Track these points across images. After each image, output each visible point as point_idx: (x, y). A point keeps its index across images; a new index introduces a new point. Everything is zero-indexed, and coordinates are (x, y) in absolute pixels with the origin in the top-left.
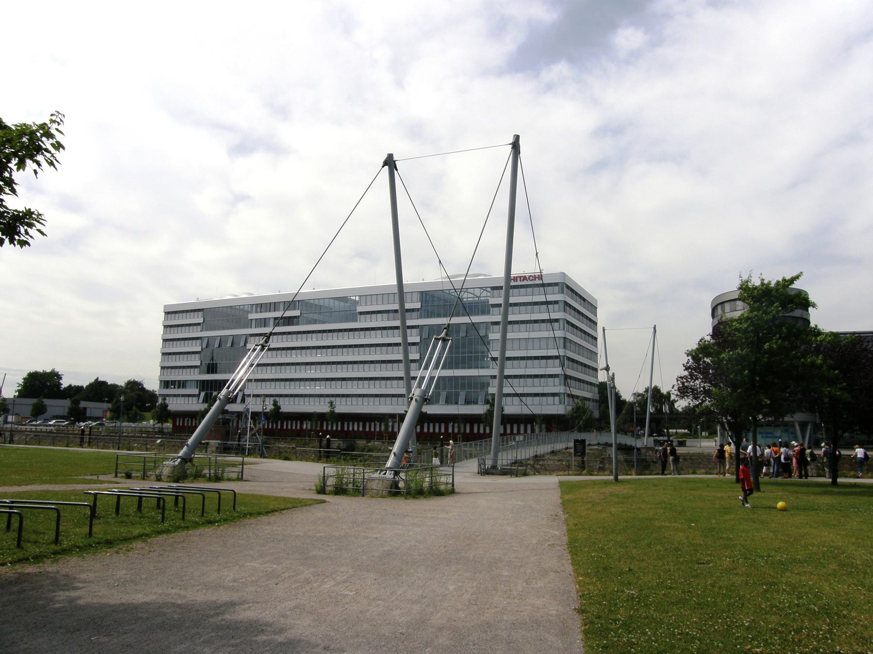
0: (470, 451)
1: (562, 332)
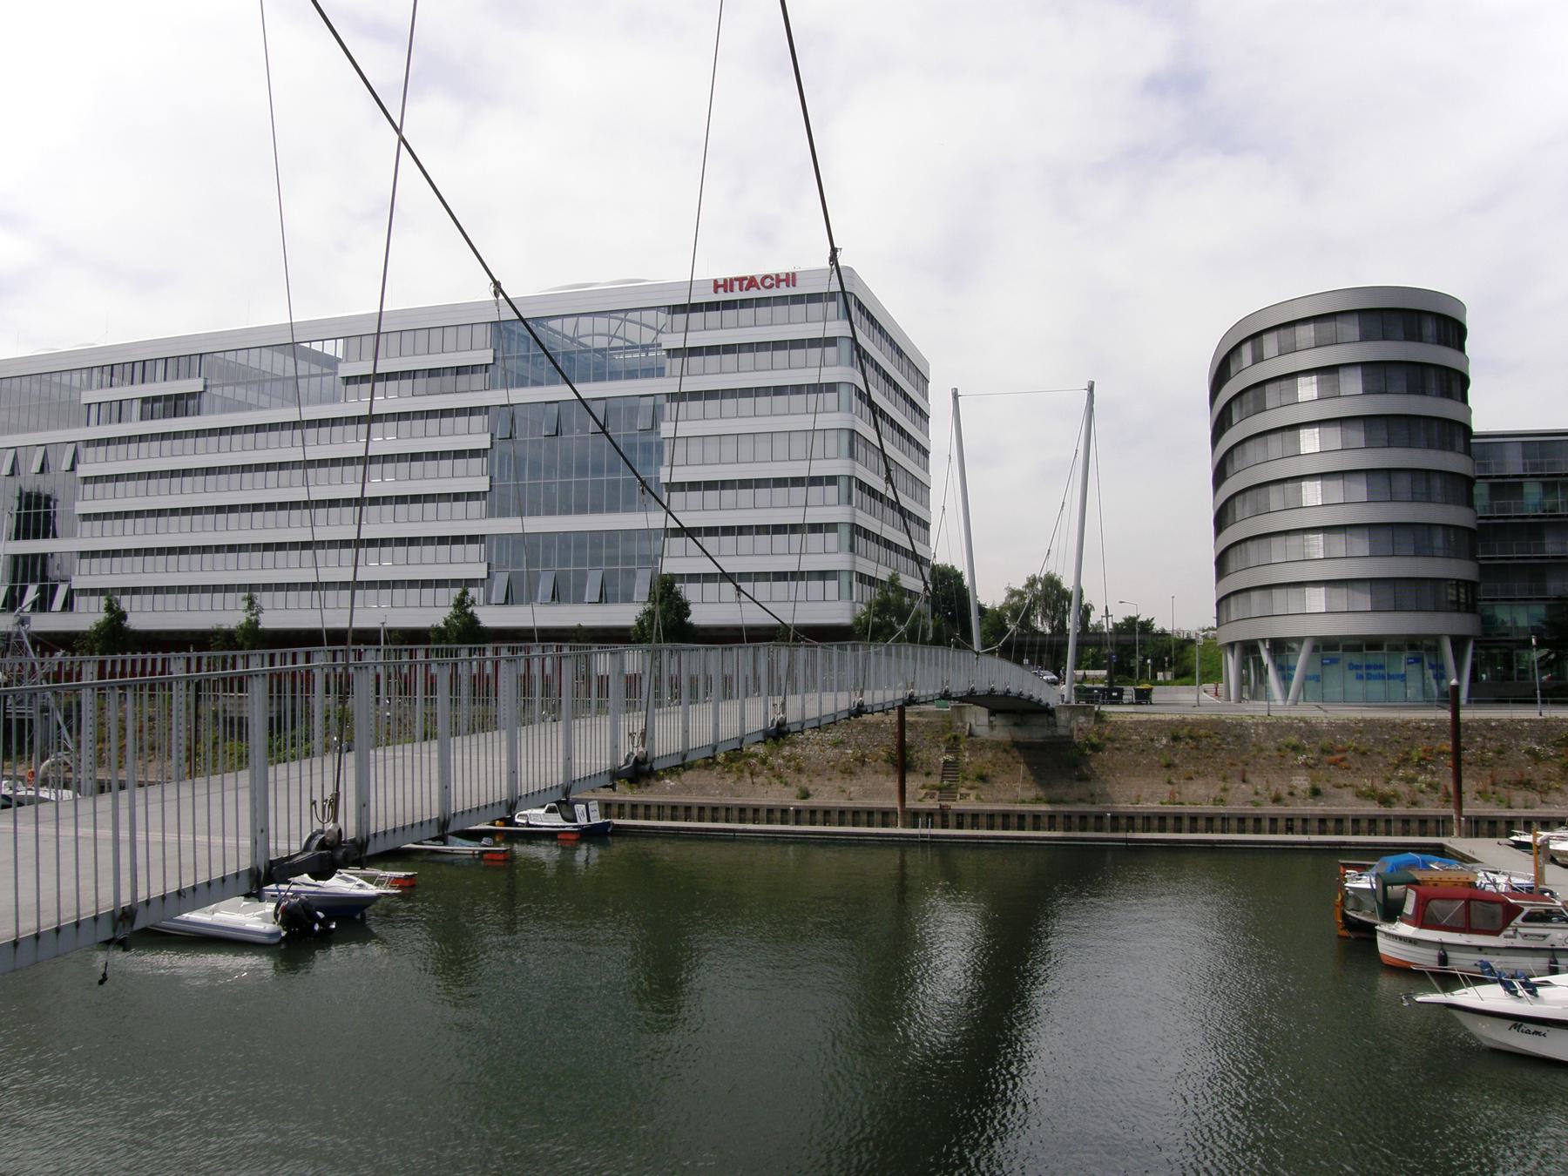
1: (847, 416)
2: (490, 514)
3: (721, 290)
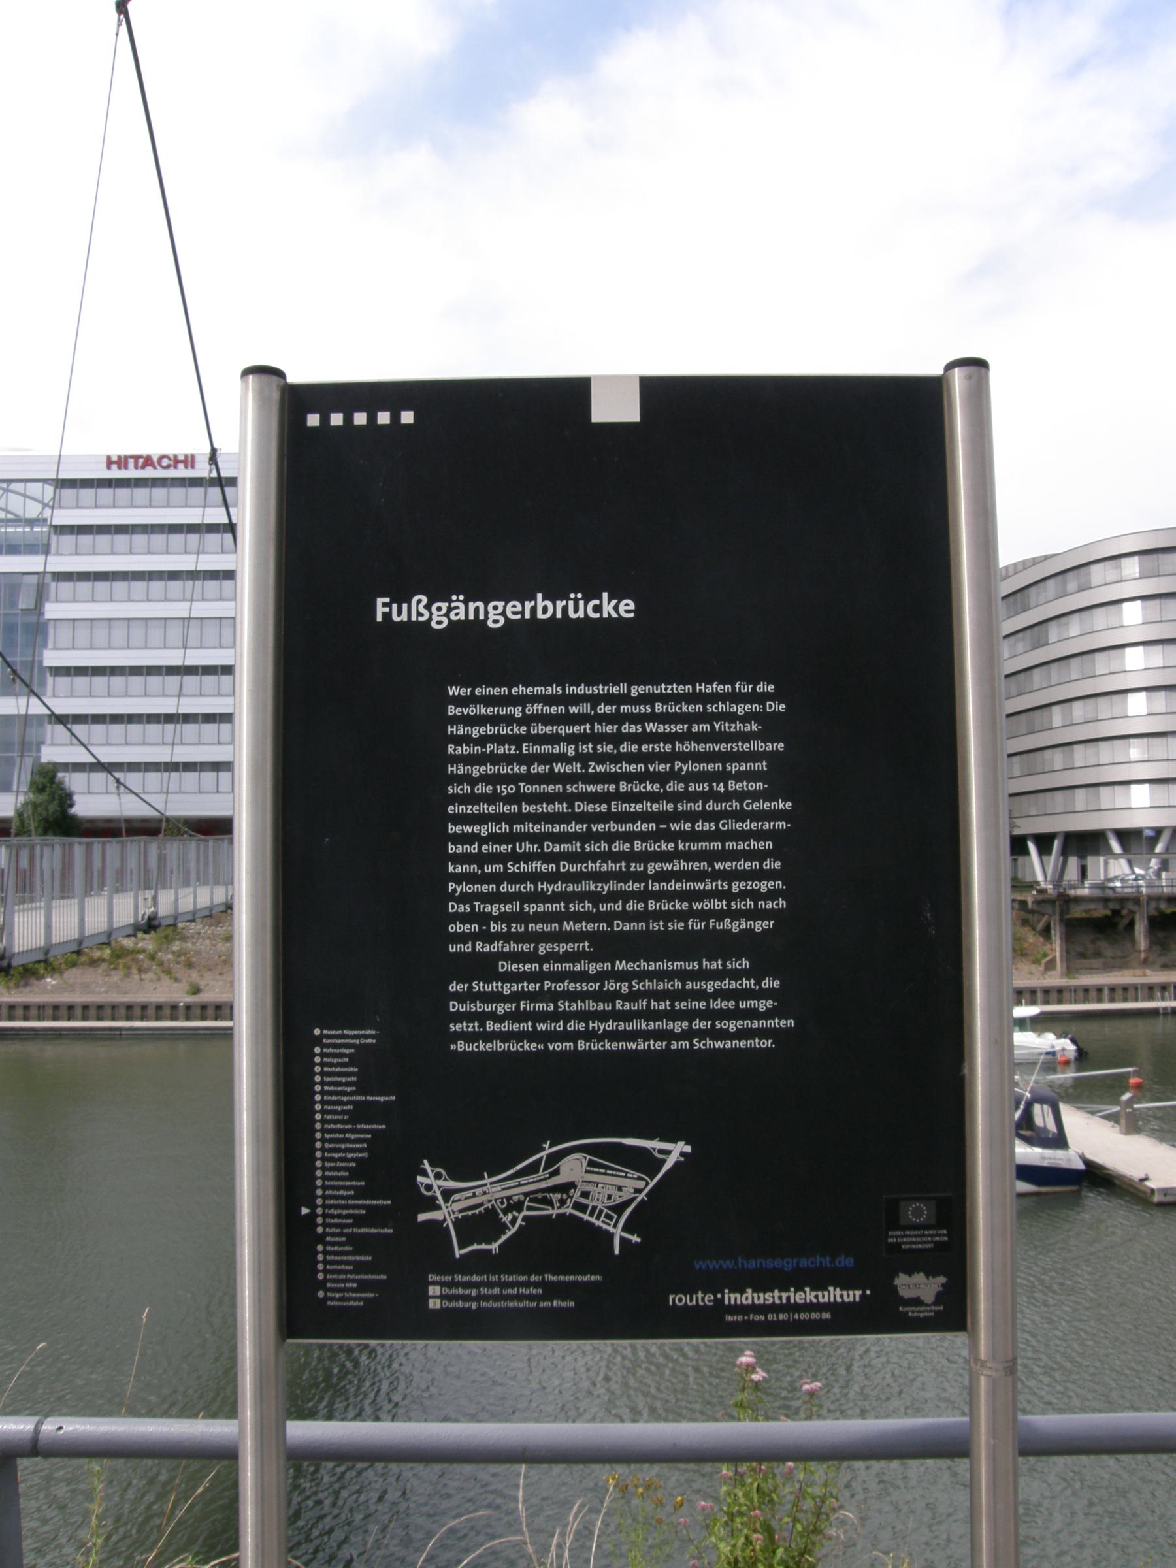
3: (114, 467)
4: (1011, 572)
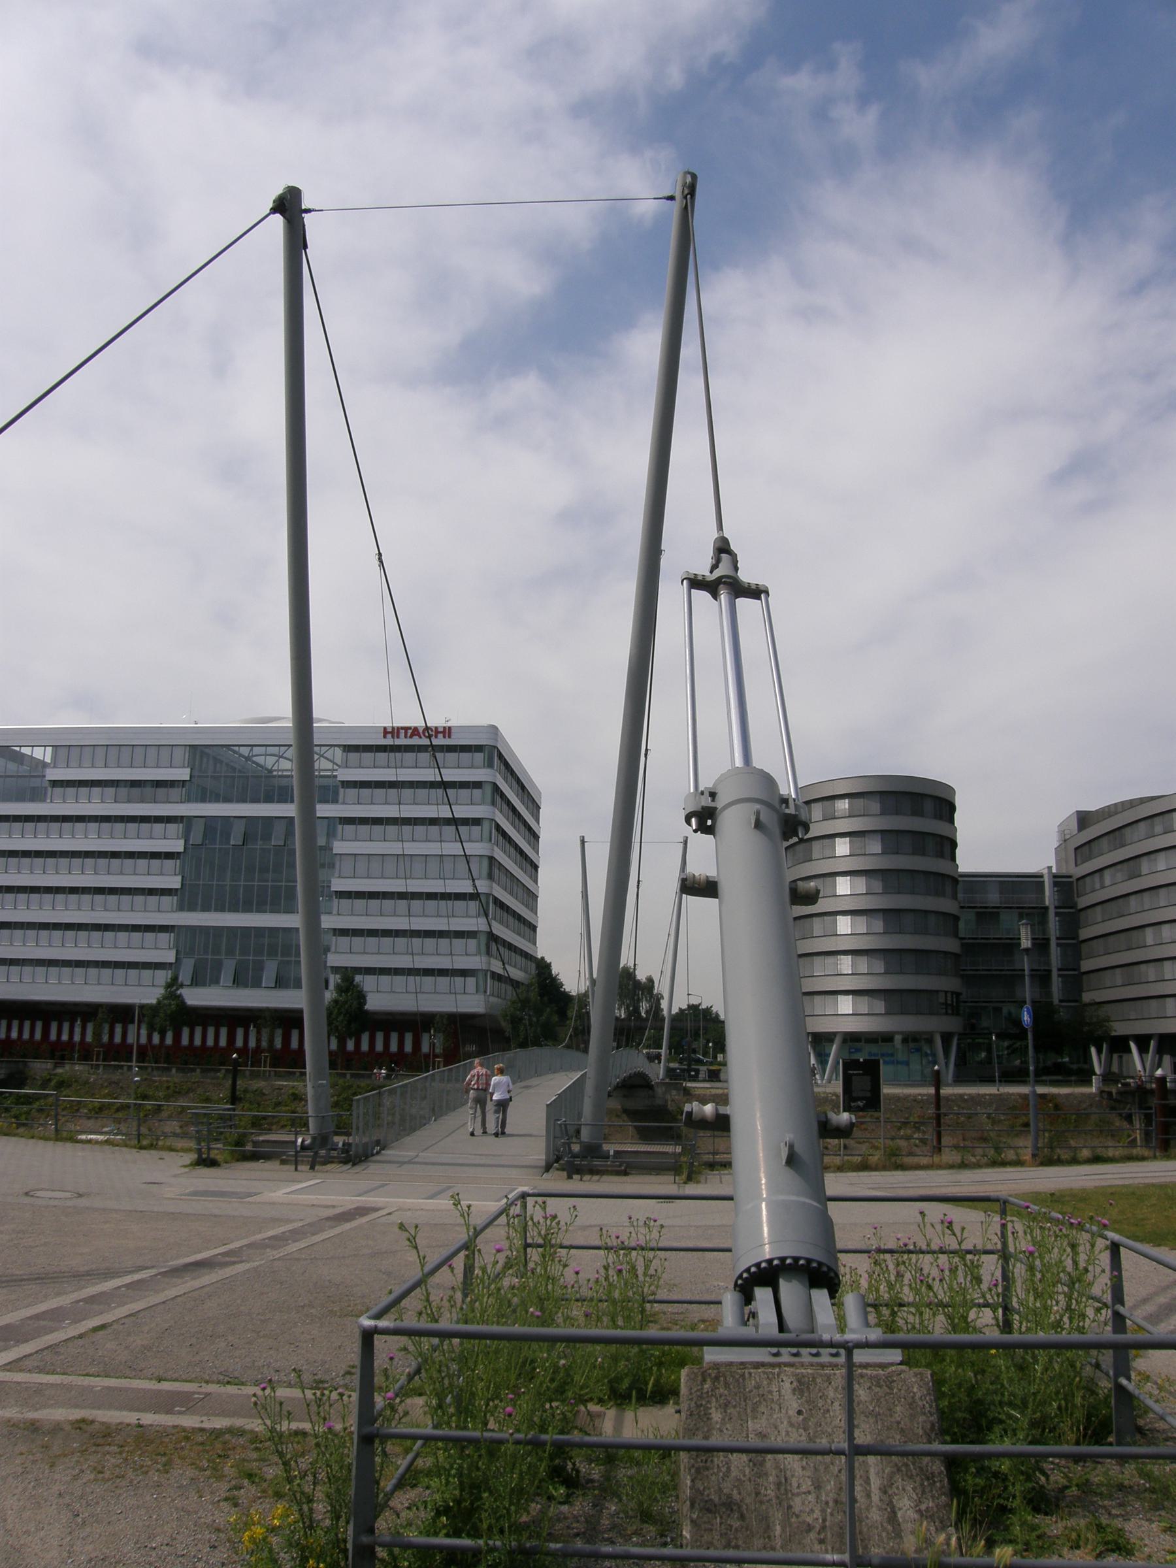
0: (167, 1081)
2: (181, 908)
3: (389, 736)
4: (1120, 809)
